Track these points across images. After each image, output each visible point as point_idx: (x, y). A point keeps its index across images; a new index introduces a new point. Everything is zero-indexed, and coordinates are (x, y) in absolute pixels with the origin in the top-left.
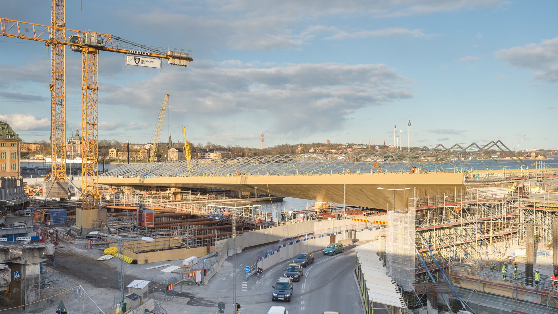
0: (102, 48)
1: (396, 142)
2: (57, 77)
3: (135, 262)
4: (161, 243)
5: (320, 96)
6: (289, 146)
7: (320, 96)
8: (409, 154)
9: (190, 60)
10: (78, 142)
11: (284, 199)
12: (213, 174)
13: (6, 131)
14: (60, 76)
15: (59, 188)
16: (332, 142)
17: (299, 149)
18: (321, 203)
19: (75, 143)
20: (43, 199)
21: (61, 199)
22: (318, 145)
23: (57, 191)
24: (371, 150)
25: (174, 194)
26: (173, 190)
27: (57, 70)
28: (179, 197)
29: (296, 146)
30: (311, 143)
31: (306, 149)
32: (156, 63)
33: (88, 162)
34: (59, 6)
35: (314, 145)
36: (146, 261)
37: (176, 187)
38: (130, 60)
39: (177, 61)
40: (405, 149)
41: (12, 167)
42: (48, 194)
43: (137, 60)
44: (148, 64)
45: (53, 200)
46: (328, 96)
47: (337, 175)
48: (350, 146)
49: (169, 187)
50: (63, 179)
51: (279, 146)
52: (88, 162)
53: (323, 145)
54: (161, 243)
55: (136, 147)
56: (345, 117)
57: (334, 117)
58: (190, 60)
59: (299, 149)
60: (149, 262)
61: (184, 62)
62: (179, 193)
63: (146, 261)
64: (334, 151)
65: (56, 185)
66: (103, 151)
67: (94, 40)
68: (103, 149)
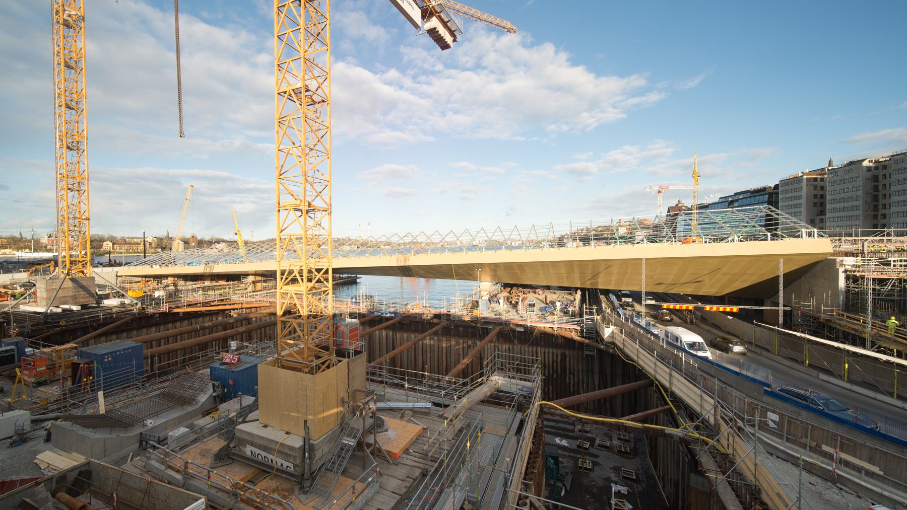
2: (71, 187)
11: (358, 280)
14: (76, 185)
15: (75, 288)
20: (41, 309)
21: (82, 306)
23: (71, 294)
25: (254, 282)
26: (251, 279)
27: (70, 174)
28: (259, 286)
33: (432, 342)
34: (72, 149)
37: (256, 274)
42: (53, 302)
45: (64, 310)
49: (246, 275)
50: (83, 272)
52: (432, 342)
62: (258, 282)
65: (69, 284)
66: (94, 244)
68: (97, 243)
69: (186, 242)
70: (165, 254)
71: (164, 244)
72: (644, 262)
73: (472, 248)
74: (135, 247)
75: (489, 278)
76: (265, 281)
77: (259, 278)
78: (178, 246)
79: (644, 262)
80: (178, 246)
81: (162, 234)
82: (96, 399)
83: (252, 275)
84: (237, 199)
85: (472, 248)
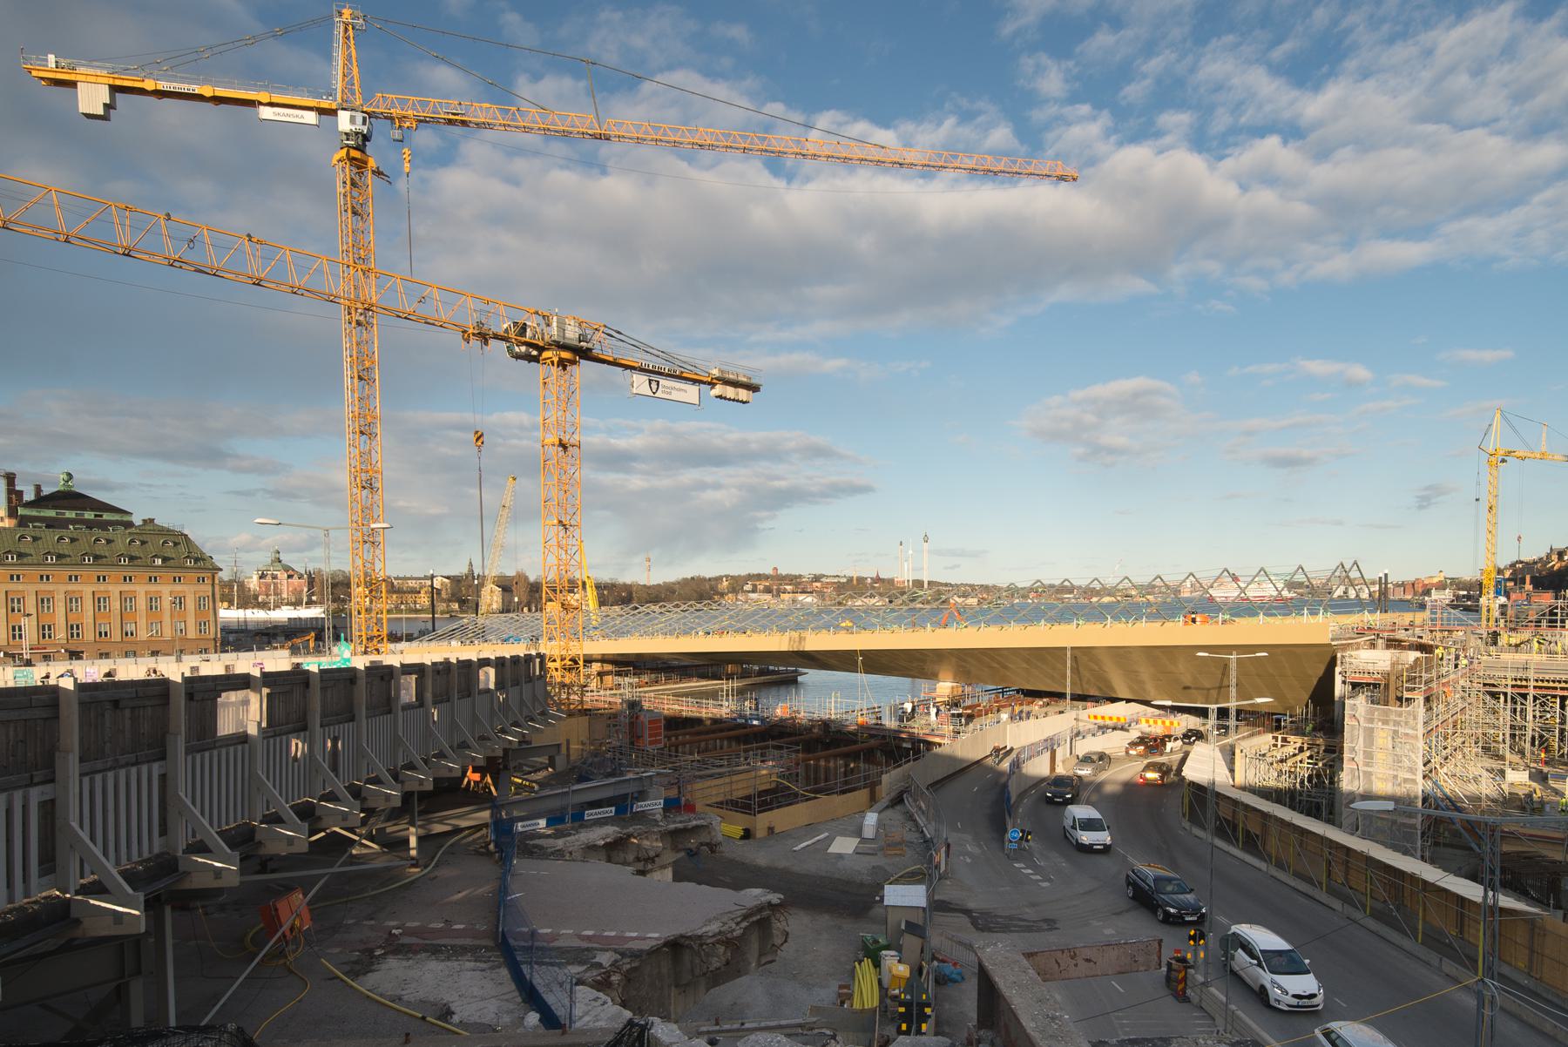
0: (585, 354)
1: (904, 574)
3: (747, 834)
4: (741, 785)
5: (703, 486)
6: (704, 580)
7: (703, 486)
8: (926, 593)
9: (754, 388)
10: (282, 575)
12: (722, 632)
13: (182, 548)
16: (783, 571)
17: (725, 584)
18: (949, 684)
19: (274, 577)
22: (759, 577)
24: (856, 586)
25: (601, 674)
26: (596, 667)
28: (609, 679)
29: (719, 579)
30: (743, 573)
31: (737, 584)
32: (690, 393)
35: (750, 577)
36: (771, 830)
37: (604, 659)
38: (640, 382)
39: (730, 392)
40: (918, 584)
41: (201, 625)
43: (654, 385)
44: (675, 396)
46: (717, 486)
47: (993, 629)
48: (817, 578)
51: (685, 580)
53: (767, 577)
54: (741, 785)
55: (412, 584)
56: (760, 526)
57: (738, 525)
58: (754, 388)
59: (725, 584)
60: (777, 830)
61: (743, 394)
63: (771, 830)
64: (789, 588)
67: (572, 334)
69: (506, 586)
70: (467, 619)
71: (463, 592)
72: (71, 720)
73: (1245, 608)
74: (410, 598)
75: (951, 676)
76: (619, 674)
77: (608, 667)
78: (491, 597)
79: (71, 720)
80: (491, 597)
81: (460, 569)
82: (928, 714)
83: (597, 661)
84: (709, 479)
85: (1245, 608)
